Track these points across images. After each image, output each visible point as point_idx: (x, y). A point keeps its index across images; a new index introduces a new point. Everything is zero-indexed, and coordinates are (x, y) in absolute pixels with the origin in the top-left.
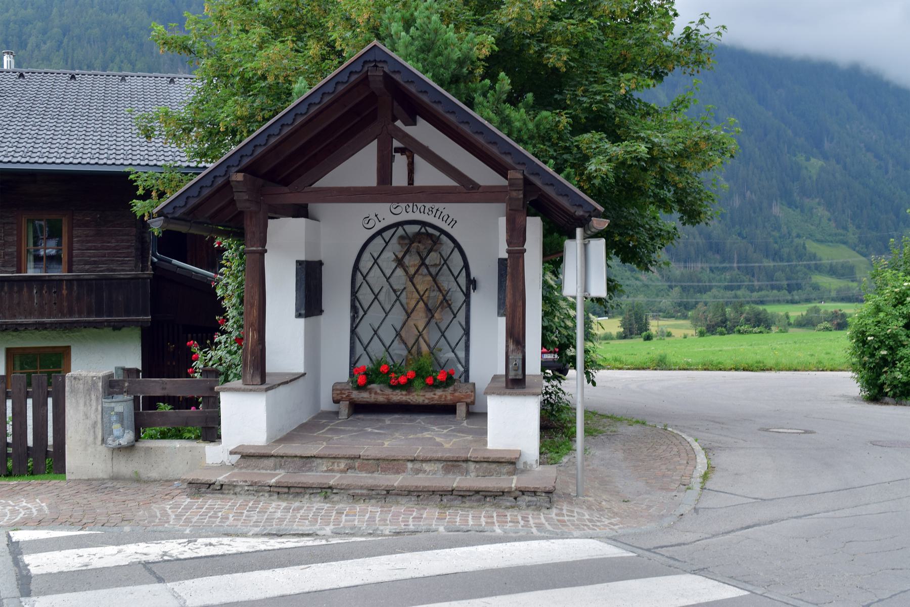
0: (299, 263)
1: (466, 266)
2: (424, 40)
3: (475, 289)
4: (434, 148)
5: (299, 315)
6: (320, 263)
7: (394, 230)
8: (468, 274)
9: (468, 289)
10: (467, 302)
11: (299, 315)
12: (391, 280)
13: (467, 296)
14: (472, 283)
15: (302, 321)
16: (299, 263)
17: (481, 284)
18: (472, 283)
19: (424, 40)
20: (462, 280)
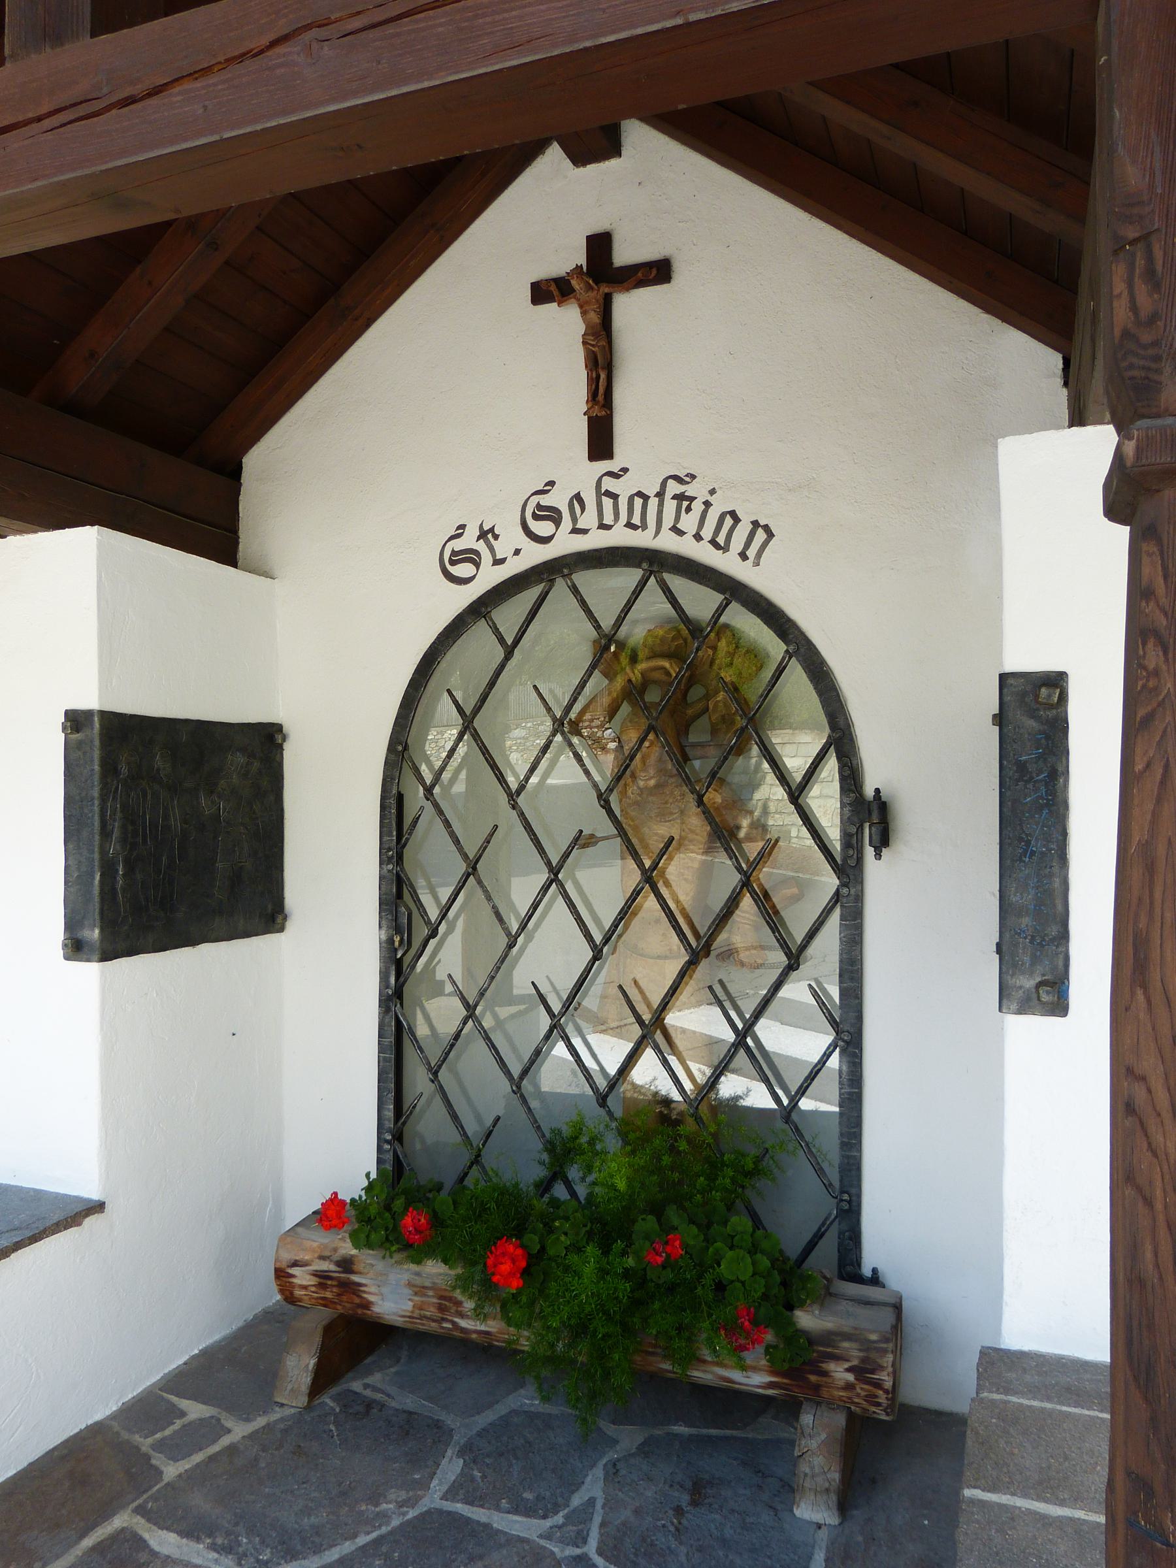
0: (75, 721)
1: (841, 741)
2: (580, 1319)
3: (883, 841)
4: (588, 1053)
5: (76, 948)
6: (266, 740)
7: (534, 593)
8: (851, 777)
9: (851, 841)
10: (849, 902)
11: (76, 948)
12: (521, 800)
13: (849, 870)
14: (872, 818)
15: (90, 971)
16: (75, 721)
17: (910, 818)
18: (872, 818)
19: (580, 1319)
20: (826, 802)
